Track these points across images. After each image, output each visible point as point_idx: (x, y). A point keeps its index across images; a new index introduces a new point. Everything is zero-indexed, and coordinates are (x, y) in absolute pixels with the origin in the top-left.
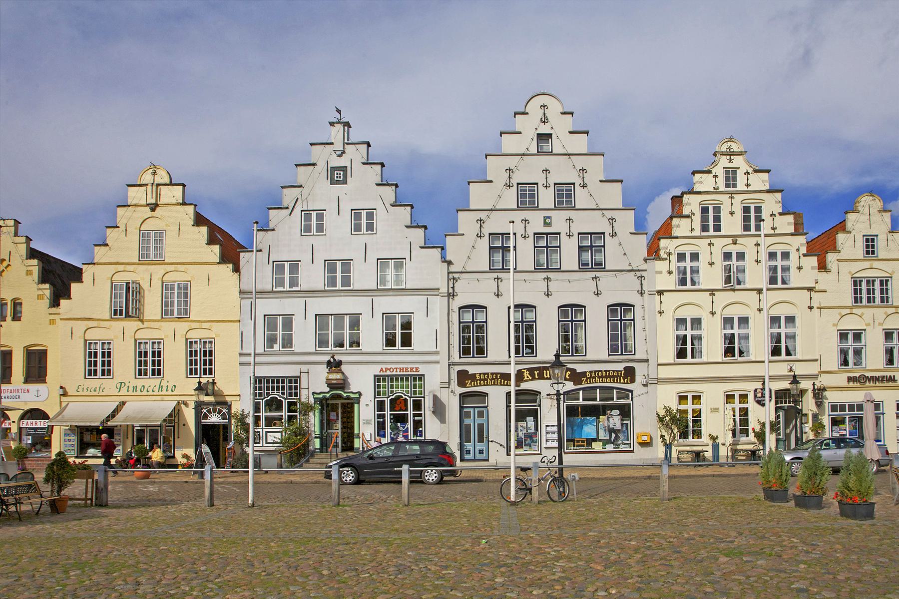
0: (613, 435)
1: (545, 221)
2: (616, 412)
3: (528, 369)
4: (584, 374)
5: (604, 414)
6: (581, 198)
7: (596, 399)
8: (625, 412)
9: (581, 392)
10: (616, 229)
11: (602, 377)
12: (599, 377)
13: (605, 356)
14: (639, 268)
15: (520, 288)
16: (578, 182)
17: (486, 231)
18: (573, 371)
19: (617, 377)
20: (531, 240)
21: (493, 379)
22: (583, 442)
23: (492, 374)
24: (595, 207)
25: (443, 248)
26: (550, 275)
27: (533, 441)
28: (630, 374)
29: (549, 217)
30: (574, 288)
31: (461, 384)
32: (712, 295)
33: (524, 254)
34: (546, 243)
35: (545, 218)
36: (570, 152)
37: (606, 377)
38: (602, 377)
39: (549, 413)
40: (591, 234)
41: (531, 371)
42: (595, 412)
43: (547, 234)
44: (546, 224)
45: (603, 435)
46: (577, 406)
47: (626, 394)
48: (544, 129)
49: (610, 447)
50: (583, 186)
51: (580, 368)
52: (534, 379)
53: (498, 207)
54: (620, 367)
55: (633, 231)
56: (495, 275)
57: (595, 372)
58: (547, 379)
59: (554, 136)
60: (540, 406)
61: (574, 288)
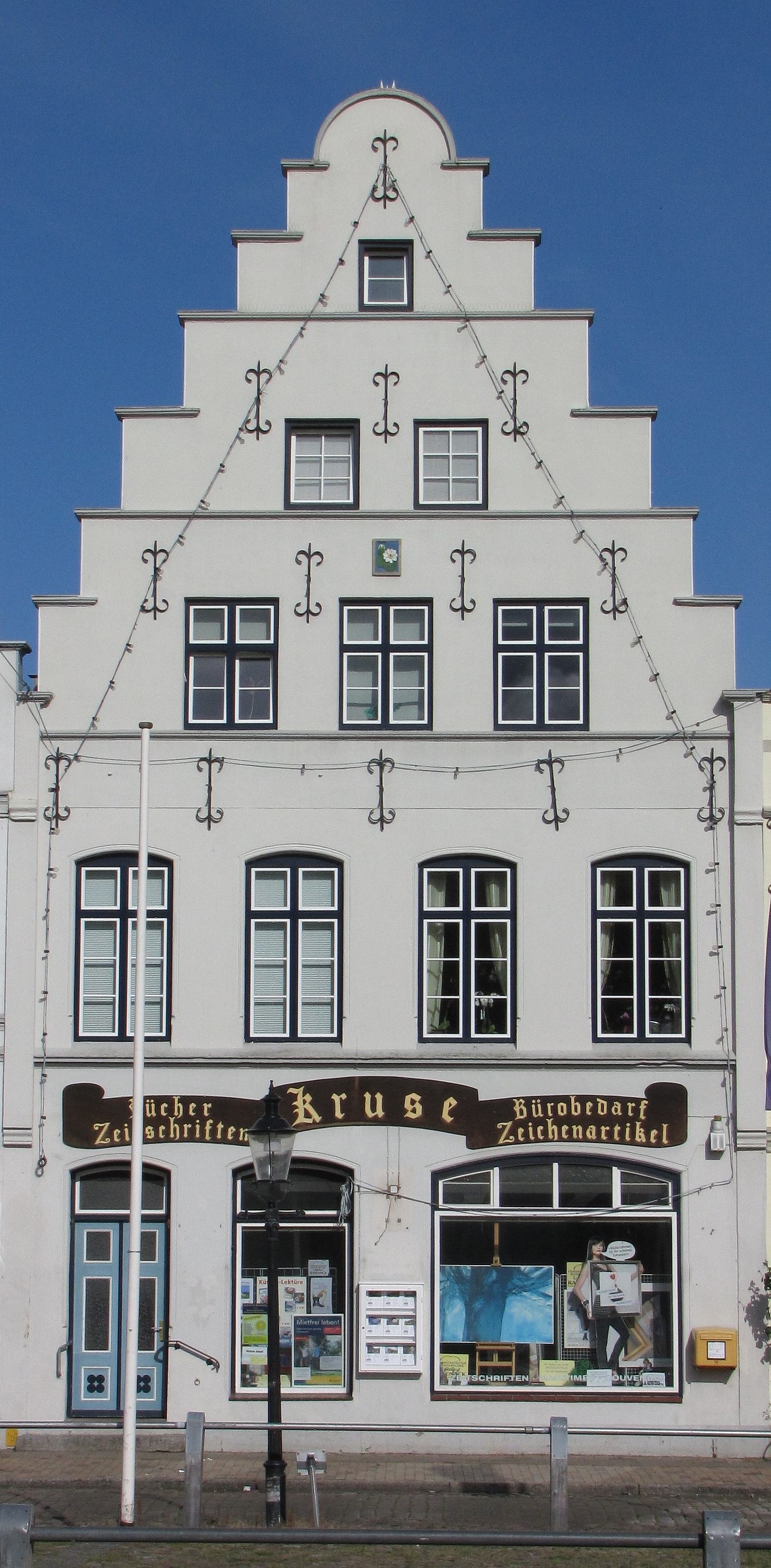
0: (613, 1336)
1: (379, 554)
2: (621, 1250)
3: (309, 1087)
4: (504, 1108)
5: (581, 1256)
6: (513, 480)
7: (546, 1201)
8: (654, 1249)
9: (495, 1173)
10: (629, 588)
11: (569, 1120)
12: (559, 1121)
13: (580, 1043)
14: (703, 729)
15: (285, 792)
16: (498, 416)
17: (177, 585)
18: (466, 1095)
19: (623, 1120)
20: (327, 625)
21: (186, 1118)
22: (505, 1355)
23: (186, 1100)
24: (548, 506)
25: (25, 650)
26: (392, 749)
27: (325, 1350)
28: (666, 1109)
29: (394, 544)
30: (471, 792)
31: (77, 1132)
32: (52, 790)
33: (310, 674)
34: (387, 642)
35: (381, 546)
36: (471, 307)
37: (584, 1120)
38: (569, 1120)
39: (395, 1252)
40: (232, 602)
41: (320, 1092)
42: (566, 1245)
43: (386, 603)
44: (385, 568)
45: (575, 1335)
46: (487, 1225)
47: (663, 1184)
48: (386, 225)
49: (600, 1380)
50: (516, 432)
51: (490, 1086)
52: (328, 1120)
53: (214, 506)
54: (634, 1085)
55: (688, 593)
56: (201, 748)
57: (545, 1100)
58: (376, 1122)
59: (419, 252)
60: (350, 1219)
61: (471, 792)
